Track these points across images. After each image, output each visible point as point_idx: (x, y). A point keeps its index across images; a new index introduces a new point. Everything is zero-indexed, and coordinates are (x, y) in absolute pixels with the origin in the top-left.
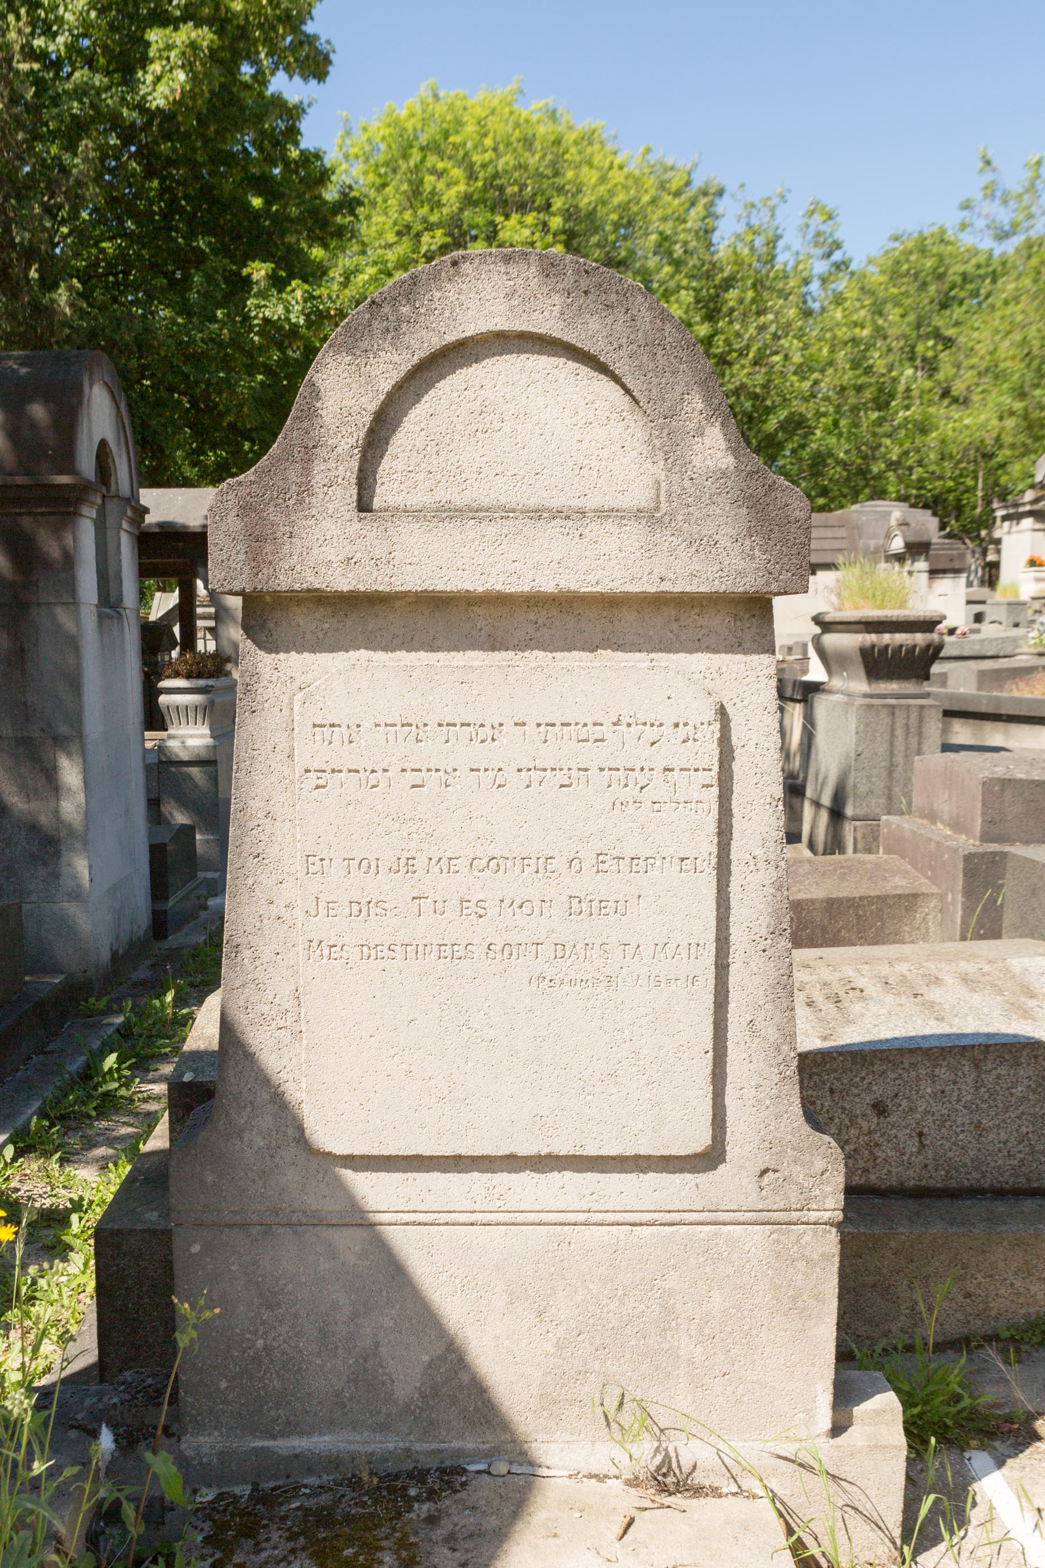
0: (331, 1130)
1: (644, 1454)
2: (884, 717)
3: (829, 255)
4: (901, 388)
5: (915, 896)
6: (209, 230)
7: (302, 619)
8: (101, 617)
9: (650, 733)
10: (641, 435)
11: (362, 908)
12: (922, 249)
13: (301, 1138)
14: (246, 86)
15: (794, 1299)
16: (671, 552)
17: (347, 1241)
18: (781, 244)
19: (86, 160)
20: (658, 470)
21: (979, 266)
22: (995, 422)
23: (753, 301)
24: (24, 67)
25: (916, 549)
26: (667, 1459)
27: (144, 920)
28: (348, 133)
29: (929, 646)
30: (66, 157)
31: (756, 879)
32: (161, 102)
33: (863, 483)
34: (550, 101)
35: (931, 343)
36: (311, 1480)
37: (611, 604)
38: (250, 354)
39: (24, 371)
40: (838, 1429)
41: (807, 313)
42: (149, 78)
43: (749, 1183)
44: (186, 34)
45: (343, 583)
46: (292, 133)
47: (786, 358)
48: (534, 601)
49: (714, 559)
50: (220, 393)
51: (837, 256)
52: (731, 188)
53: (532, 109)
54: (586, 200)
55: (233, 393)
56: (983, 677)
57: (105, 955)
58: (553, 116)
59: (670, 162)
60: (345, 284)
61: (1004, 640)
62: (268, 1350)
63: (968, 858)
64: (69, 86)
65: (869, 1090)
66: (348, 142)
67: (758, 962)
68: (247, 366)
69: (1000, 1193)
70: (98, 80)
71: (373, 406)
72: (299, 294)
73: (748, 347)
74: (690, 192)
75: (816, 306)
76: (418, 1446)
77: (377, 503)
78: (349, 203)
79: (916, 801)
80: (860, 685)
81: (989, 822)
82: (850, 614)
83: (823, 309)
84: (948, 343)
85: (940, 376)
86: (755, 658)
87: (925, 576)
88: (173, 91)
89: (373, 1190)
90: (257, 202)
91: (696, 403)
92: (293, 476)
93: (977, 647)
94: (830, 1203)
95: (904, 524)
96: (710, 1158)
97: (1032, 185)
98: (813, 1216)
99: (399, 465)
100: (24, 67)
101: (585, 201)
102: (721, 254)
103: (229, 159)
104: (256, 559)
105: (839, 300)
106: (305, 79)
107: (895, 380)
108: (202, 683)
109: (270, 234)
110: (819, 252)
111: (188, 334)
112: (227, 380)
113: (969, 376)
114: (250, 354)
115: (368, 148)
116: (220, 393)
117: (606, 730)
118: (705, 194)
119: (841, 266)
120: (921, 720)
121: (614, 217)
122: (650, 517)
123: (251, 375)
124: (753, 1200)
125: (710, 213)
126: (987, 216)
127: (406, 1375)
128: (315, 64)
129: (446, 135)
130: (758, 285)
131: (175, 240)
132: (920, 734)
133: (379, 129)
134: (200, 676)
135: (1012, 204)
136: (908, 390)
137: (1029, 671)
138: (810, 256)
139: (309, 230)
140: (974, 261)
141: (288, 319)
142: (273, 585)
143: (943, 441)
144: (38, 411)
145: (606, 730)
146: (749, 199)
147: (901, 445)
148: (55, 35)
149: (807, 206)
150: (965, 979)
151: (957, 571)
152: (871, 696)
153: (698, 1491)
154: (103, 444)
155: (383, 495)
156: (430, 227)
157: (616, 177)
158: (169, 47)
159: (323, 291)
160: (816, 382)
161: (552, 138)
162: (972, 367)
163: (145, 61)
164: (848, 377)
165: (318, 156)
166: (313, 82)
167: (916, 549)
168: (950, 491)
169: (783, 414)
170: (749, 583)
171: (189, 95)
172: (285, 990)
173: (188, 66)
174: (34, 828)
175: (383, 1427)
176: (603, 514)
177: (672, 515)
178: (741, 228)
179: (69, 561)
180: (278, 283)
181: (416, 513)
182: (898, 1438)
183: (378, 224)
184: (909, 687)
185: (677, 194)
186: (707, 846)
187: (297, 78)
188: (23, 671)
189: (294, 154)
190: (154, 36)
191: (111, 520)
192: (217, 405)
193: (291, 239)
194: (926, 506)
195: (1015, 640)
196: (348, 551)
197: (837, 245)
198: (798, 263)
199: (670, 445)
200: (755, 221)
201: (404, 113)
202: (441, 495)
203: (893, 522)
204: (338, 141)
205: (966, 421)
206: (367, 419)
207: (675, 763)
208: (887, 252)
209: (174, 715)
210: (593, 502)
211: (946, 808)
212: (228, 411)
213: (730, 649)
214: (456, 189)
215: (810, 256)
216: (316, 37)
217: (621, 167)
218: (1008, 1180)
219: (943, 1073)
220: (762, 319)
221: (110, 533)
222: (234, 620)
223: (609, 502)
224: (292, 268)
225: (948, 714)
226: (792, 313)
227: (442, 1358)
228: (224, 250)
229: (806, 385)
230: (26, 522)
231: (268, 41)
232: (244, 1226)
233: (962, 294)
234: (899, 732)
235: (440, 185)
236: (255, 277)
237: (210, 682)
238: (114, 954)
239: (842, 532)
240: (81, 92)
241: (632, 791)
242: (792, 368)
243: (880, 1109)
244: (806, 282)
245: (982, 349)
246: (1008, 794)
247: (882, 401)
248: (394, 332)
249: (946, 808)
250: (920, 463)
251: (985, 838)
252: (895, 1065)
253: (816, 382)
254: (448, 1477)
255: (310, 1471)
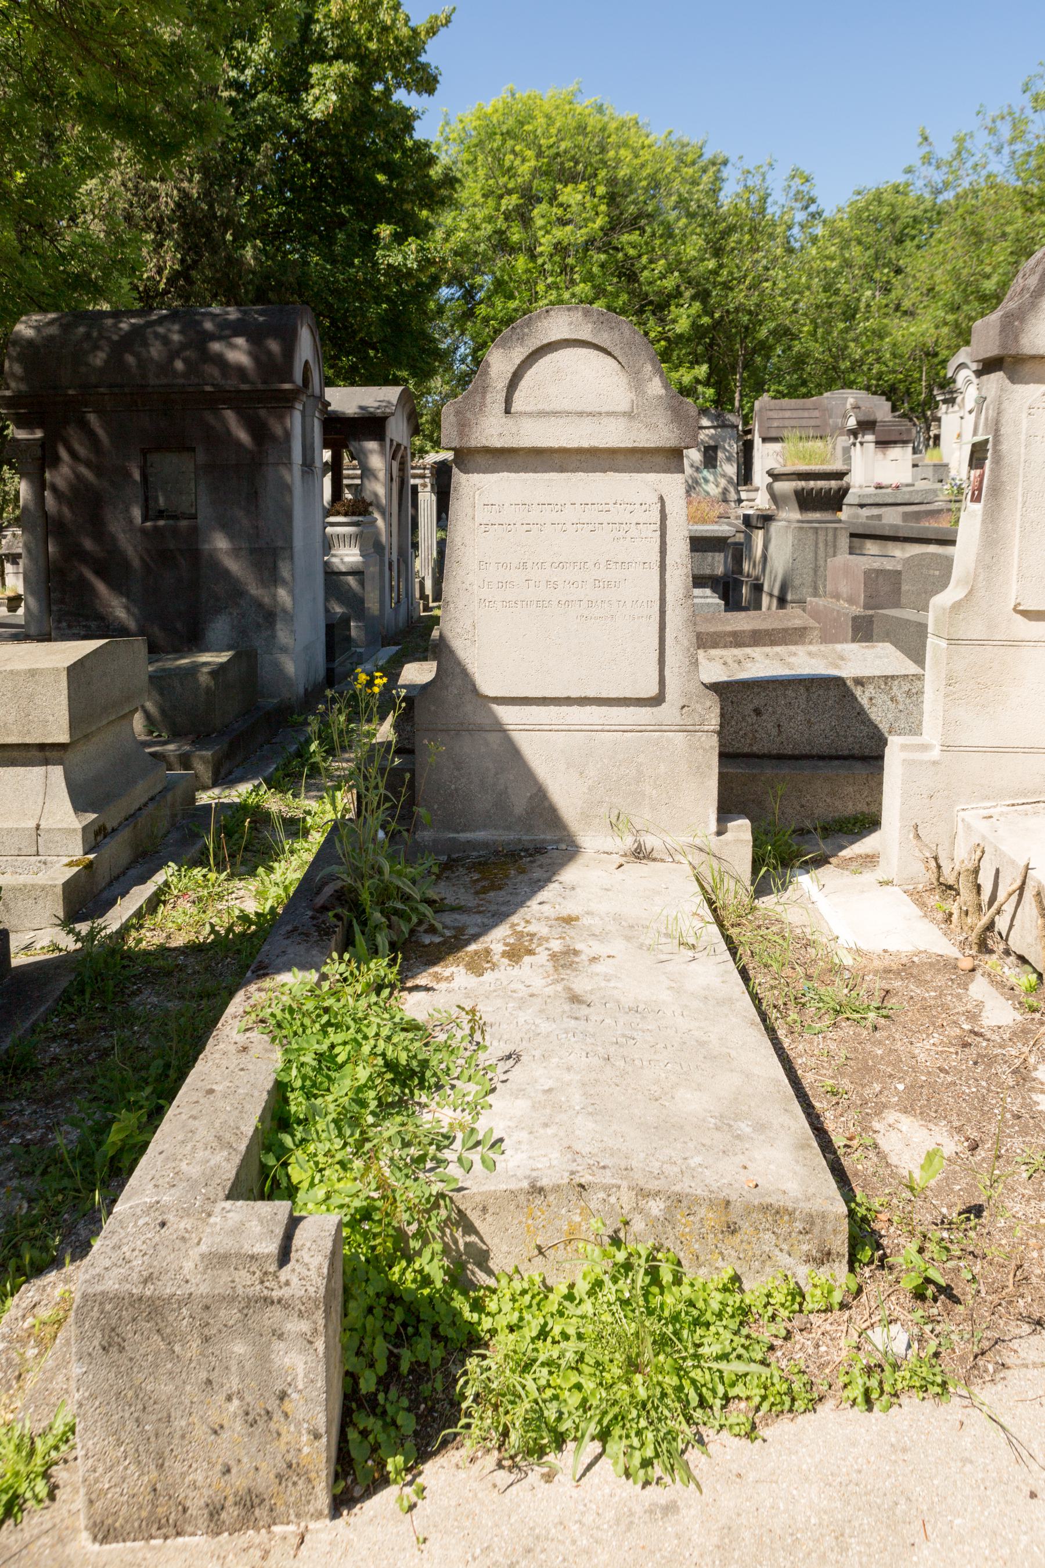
0: (488, 687)
1: (628, 842)
2: (811, 535)
3: (806, 208)
4: (862, 305)
5: (805, 628)
6: (349, 200)
7: (480, 459)
8: (303, 473)
9: (630, 508)
10: (625, 381)
11: (503, 585)
12: (878, 199)
13: (475, 690)
14: (377, 100)
15: (698, 768)
16: (639, 430)
17: (493, 738)
18: (770, 200)
19: (266, 156)
20: (633, 396)
21: (926, 211)
22: (932, 330)
23: (749, 243)
24: (225, 94)
25: (866, 425)
26: (640, 845)
27: (322, 673)
28: (447, 124)
29: (839, 489)
30: (251, 155)
31: (678, 572)
32: (319, 115)
33: (835, 377)
34: (598, 98)
35: (886, 271)
36: (475, 854)
37: (613, 452)
38: (377, 289)
39: (261, 319)
40: (719, 833)
41: (790, 251)
42: (311, 98)
43: (676, 711)
44: (338, 68)
45: (498, 444)
46: (409, 128)
47: (774, 284)
48: (580, 451)
49: (658, 433)
50: (355, 317)
51: (813, 208)
52: (733, 159)
53: (585, 105)
54: (622, 173)
55: (364, 316)
56: (906, 516)
57: (301, 691)
58: (600, 110)
59: (685, 140)
60: (446, 240)
61: (927, 491)
62: (456, 790)
63: (855, 619)
64: (254, 104)
65: (751, 701)
66: (447, 129)
67: (679, 609)
68: (374, 297)
69: (821, 758)
70: (275, 100)
71: (512, 370)
72: (413, 247)
73: (745, 276)
74: (702, 163)
75: (797, 245)
76: (524, 838)
77: (513, 410)
78: (450, 181)
79: (829, 588)
80: (795, 515)
81: (869, 597)
82: (789, 469)
83: (802, 247)
84: (898, 271)
85: (893, 295)
86: (676, 475)
87: (873, 445)
88: (327, 107)
89: (506, 714)
90: (381, 178)
91: (649, 368)
92: (478, 399)
93: (907, 496)
94: (714, 722)
95: (856, 407)
96: (658, 700)
97: (959, 153)
98: (706, 728)
99: (523, 394)
100: (225, 94)
101: (623, 173)
102: (725, 208)
103: (364, 151)
104: (462, 434)
105: (814, 240)
106: (419, 93)
107: (858, 300)
108: (355, 519)
109: (392, 203)
110: (799, 205)
111: (333, 276)
112: (361, 308)
113: (914, 296)
114: (377, 289)
115: (463, 135)
116: (355, 317)
117: (611, 507)
118: (714, 164)
119: (818, 214)
120: (835, 537)
121: (644, 183)
122: (629, 415)
123: (379, 304)
124: (678, 720)
125: (718, 179)
126: (925, 177)
127: (519, 804)
128: (427, 83)
129: (522, 124)
130: (754, 230)
131: (324, 208)
132: (835, 546)
133: (472, 123)
134: (353, 514)
135: (944, 169)
136: (868, 306)
137: (939, 512)
138: (792, 209)
139: (421, 200)
140: (922, 207)
141: (405, 265)
142: (468, 445)
143: (895, 345)
144: (274, 346)
145: (611, 507)
146: (746, 167)
147: (863, 347)
148: (244, 68)
149: (789, 172)
150: (810, 654)
151: (905, 442)
152: (802, 522)
153: (654, 860)
154: (307, 362)
155: (516, 407)
156: (509, 192)
157: (645, 155)
158: (325, 77)
159: (432, 245)
160: (796, 302)
161: (599, 126)
162: (917, 289)
163: (307, 87)
164: (822, 297)
165: (427, 145)
166: (425, 96)
167: (866, 425)
168: (900, 381)
169: (772, 325)
170: (672, 443)
171: (339, 109)
172: (469, 622)
173: (338, 90)
174: (260, 605)
175: (509, 828)
176: (609, 414)
177: (639, 414)
178: (739, 189)
179: (288, 435)
180: (399, 239)
181: (530, 414)
182: (748, 836)
183: (470, 191)
184: (827, 516)
185: (693, 163)
186: (656, 557)
187: (413, 93)
188: (257, 506)
189: (410, 143)
190: (315, 69)
191: (308, 412)
192: (352, 325)
193: (407, 206)
194: (883, 394)
195: (934, 492)
196: (500, 430)
197: (813, 201)
198: (783, 213)
199: (637, 384)
200: (749, 183)
201: (489, 110)
202: (540, 407)
203: (848, 406)
204: (440, 128)
205: (912, 330)
206: (510, 375)
207: (641, 521)
208: (852, 204)
209: (335, 541)
210: (603, 410)
211: (844, 590)
212: (360, 330)
213: (665, 471)
214: (528, 164)
215: (792, 209)
216: (428, 65)
217: (650, 147)
218: (827, 752)
219: (789, 693)
220: (756, 256)
221: (308, 419)
222: (376, 478)
223: (611, 409)
224: (411, 228)
225: (853, 535)
226: (779, 251)
227: (536, 795)
228: (359, 215)
229: (789, 303)
230: (263, 413)
231: (393, 68)
232: (447, 731)
233: (913, 232)
234: (821, 545)
235: (517, 162)
236: (382, 235)
237: (360, 518)
238: (306, 690)
239: (816, 413)
240: (262, 109)
241: (622, 533)
242: (778, 292)
243: (758, 712)
244: (790, 228)
245: (922, 277)
246: (881, 579)
247: (850, 314)
248: (521, 339)
249: (844, 590)
250: (878, 360)
251: (866, 607)
252: (765, 689)
253: (796, 302)
254: (539, 850)
255: (474, 849)
